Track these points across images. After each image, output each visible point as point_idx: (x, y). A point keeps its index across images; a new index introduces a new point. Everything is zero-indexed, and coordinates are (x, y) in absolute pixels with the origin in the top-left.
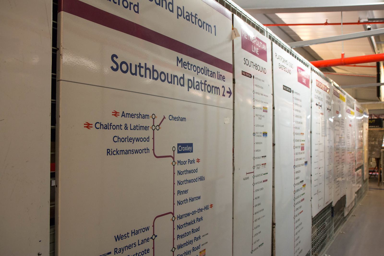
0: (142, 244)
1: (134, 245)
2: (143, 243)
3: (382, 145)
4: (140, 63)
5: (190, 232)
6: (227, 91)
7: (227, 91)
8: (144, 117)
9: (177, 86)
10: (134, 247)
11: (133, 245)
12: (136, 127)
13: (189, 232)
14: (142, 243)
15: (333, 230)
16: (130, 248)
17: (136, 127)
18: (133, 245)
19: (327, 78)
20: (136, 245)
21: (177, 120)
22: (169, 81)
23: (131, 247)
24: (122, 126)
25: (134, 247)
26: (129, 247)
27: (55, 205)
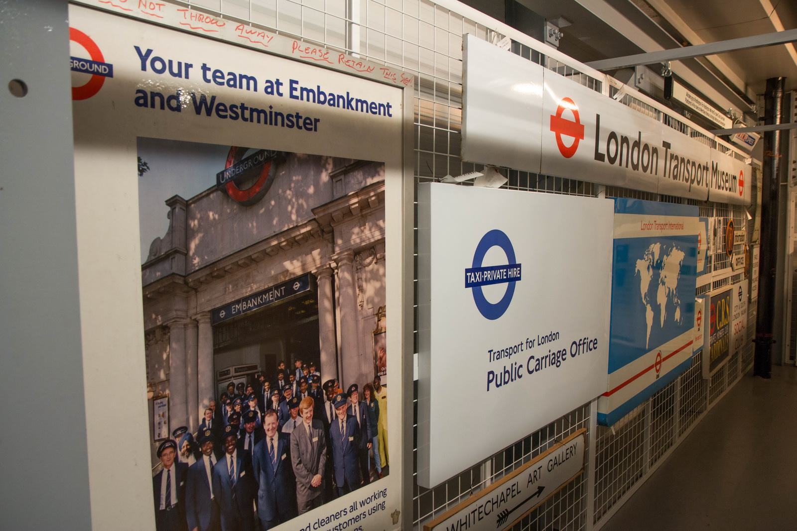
0: (536, 370)
1: (364, 515)
2: (329, 522)
3: (258, 400)
4: (247, 89)
5: (369, 515)
6: (664, 142)
7: (664, 142)
8: (334, 102)
9: (162, 110)
10: (344, 515)
11: (362, 516)
12: (275, 86)
13: (501, 385)
14: (351, 510)
15: (678, 420)
16: (337, 517)
17: (275, 86)
18: (362, 516)
19: (381, 198)
20: (365, 515)
21: (231, 117)
22: (172, 105)
23: (340, 516)
24: (282, 84)
25: (344, 515)
26: (336, 516)
27: (627, 106)
